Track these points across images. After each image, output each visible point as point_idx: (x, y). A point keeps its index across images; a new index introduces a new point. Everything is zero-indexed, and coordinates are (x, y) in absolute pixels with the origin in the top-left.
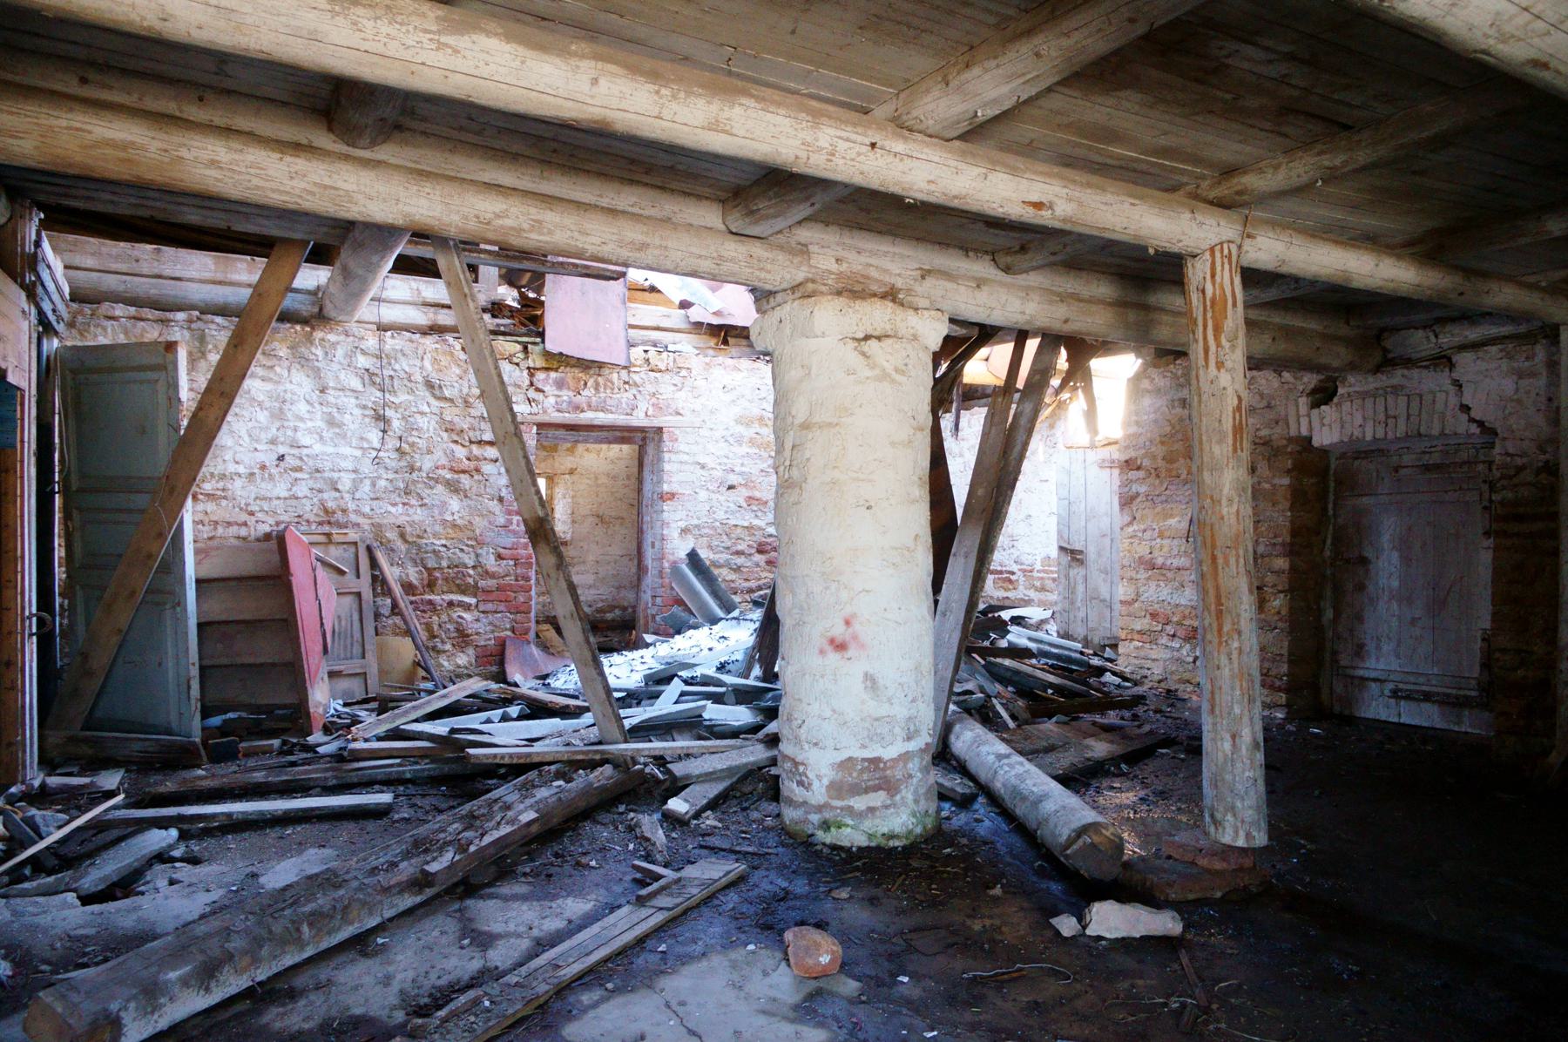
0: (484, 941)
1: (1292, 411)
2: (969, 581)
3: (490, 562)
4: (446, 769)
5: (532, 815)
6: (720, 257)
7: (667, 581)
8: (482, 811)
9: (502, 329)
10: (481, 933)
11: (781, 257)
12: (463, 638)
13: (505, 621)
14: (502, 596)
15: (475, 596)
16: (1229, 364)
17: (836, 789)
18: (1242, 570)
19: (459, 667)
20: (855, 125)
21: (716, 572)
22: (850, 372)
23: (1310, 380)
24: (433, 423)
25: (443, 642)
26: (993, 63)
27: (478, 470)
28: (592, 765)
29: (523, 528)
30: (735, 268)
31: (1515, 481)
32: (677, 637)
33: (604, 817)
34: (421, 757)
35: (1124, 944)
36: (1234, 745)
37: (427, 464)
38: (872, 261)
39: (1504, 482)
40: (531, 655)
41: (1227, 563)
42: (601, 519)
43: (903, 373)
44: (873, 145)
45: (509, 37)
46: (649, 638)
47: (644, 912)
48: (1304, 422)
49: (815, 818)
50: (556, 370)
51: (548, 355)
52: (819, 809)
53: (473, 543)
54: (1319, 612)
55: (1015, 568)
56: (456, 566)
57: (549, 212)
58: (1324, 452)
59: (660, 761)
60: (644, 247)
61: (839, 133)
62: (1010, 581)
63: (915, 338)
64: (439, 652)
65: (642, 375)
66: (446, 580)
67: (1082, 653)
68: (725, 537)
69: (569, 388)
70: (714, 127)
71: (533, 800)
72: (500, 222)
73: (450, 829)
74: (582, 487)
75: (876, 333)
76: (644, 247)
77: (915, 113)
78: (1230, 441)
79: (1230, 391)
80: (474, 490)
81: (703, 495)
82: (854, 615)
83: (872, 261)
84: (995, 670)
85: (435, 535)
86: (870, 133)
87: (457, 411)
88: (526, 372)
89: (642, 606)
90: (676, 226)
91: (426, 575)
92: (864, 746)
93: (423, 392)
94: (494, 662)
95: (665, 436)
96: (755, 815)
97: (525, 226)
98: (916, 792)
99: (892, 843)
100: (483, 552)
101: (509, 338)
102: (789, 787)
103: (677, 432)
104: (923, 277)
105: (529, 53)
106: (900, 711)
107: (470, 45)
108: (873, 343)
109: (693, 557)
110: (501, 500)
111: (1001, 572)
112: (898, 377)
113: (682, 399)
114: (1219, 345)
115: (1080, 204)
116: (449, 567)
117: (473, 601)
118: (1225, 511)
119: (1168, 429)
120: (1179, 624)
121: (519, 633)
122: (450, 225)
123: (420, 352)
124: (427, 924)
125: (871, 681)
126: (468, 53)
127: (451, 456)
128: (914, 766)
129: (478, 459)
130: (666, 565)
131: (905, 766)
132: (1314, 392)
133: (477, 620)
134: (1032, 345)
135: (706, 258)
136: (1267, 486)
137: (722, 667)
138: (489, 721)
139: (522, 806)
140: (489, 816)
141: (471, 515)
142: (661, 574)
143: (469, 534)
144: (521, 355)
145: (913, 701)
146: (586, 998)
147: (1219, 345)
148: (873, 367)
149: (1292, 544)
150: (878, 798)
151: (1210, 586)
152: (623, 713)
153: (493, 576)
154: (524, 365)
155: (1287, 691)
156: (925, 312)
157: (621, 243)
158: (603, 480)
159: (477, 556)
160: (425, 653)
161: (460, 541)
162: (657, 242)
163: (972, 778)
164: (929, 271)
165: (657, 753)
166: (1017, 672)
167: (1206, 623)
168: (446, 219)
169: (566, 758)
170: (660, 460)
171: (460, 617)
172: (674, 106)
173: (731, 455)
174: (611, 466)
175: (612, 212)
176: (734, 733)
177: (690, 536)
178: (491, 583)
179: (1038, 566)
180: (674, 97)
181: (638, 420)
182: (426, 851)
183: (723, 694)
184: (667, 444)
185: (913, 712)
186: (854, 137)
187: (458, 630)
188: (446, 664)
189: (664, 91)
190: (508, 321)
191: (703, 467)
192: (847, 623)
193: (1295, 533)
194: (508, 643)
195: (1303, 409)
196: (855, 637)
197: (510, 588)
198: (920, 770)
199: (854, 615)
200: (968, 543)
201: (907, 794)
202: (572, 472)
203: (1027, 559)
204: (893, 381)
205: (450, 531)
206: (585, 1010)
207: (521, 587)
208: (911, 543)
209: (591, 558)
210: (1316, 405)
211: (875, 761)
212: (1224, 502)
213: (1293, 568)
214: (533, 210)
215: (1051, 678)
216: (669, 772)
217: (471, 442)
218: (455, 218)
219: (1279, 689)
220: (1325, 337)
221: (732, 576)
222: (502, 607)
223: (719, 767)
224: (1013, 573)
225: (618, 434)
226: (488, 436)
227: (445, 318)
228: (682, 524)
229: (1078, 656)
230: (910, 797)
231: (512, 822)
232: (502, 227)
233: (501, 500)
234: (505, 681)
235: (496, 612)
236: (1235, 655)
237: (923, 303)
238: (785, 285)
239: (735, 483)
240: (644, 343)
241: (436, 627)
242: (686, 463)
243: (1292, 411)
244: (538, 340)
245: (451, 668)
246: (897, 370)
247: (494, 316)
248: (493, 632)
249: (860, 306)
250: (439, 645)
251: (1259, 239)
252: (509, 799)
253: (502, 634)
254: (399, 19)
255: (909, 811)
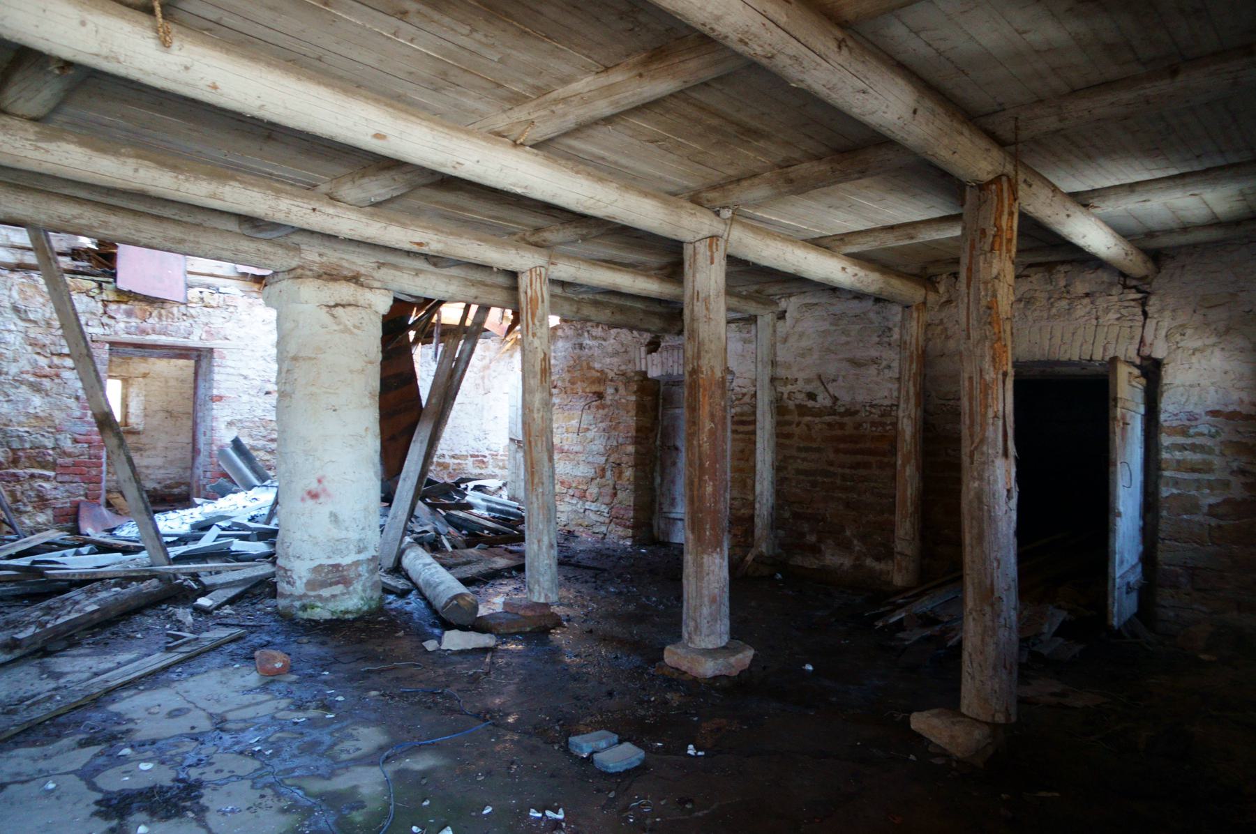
0: (58, 676)
1: (637, 356)
2: (422, 459)
3: (67, 444)
4: (28, 589)
5: (95, 607)
6: (237, 250)
7: (215, 460)
8: (57, 605)
9: (81, 269)
10: (55, 673)
11: (280, 251)
12: (42, 502)
13: (80, 489)
14: (77, 470)
15: (54, 470)
16: (539, 334)
17: (311, 585)
18: (545, 449)
19: (39, 524)
20: (303, 198)
21: (254, 454)
22: (323, 327)
23: (647, 337)
24: (19, 338)
25: (25, 505)
26: (374, 178)
27: (58, 376)
28: (141, 579)
29: (93, 420)
30: (248, 257)
31: (742, 402)
32: (220, 500)
33: (149, 612)
34: (8, 582)
35: (462, 653)
36: (539, 546)
37: (14, 369)
38: (343, 256)
39: (737, 402)
40: (101, 514)
41: (536, 445)
42: (170, 414)
43: (358, 328)
44: (314, 210)
45: (82, 144)
46: (198, 501)
47: (170, 655)
48: (643, 362)
49: (297, 604)
50: (126, 303)
51: (119, 292)
52: (300, 598)
53: (53, 430)
54: (653, 479)
55: (486, 453)
56: (38, 448)
57: (112, 216)
58: (656, 382)
59: (195, 576)
60: (182, 241)
61: (292, 202)
62: (483, 462)
63: (370, 306)
64: (21, 513)
65: (198, 310)
66: (28, 458)
67: (518, 509)
68: (262, 429)
69: (137, 317)
70: (213, 196)
71: (95, 599)
72: (77, 221)
73: (32, 615)
74: (153, 388)
75: (342, 303)
76: (182, 241)
77: (340, 193)
78: (539, 377)
79: (539, 350)
80: (54, 390)
81: (245, 398)
82: (324, 477)
83: (343, 256)
84: (452, 519)
85: (20, 424)
86: (312, 202)
87: (40, 330)
88: (100, 304)
89: (195, 479)
90: (206, 229)
91: (10, 454)
92: (329, 557)
93: (10, 315)
94: (70, 519)
95: (215, 355)
96: (260, 606)
97: (96, 225)
98: (364, 585)
99: (347, 616)
100: (61, 437)
101: (86, 277)
102: (283, 587)
103: (225, 352)
104: (379, 268)
105: (95, 154)
106: (354, 535)
107: (56, 148)
108: (340, 309)
109: (237, 444)
110: (77, 398)
111: (477, 456)
112: (356, 331)
113: (230, 328)
114: (534, 324)
115: (446, 244)
116: (31, 448)
117: (52, 474)
118: (536, 416)
119: (572, 362)
120: (576, 488)
121: (92, 498)
122: (39, 221)
123: (9, 284)
124: (16, 670)
125: (334, 518)
126: (55, 153)
127: (35, 364)
128: (363, 569)
129: (58, 367)
130: (215, 448)
131: (356, 569)
132: (650, 344)
133: (55, 488)
134: (474, 308)
135: (227, 250)
136: (623, 401)
137: (252, 519)
138: (64, 555)
139: (87, 602)
140: (63, 607)
141: (51, 409)
142: (210, 456)
143: (49, 423)
144: (97, 291)
145: (363, 529)
146: (125, 694)
147: (534, 324)
148: (339, 324)
149: (636, 437)
150: (338, 589)
151: (528, 457)
152: (169, 549)
153: (69, 455)
154: (98, 298)
155: (633, 527)
156: (378, 291)
157: (165, 238)
158: (172, 383)
159: (56, 440)
160: (9, 513)
161: (41, 428)
162: (192, 238)
163: (408, 578)
164: (383, 264)
165: (192, 571)
166: (465, 520)
168: (36, 217)
169: (123, 575)
170: (211, 372)
171: (40, 486)
172: (187, 185)
173: (268, 370)
174: (180, 372)
175: (159, 218)
176: (252, 558)
177: (234, 428)
178: (68, 460)
179: (501, 452)
180: (187, 180)
181: (194, 342)
182: (15, 627)
183: (248, 535)
184: (217, 360)
185: (363, 536)
186: (301, 204)
187: (38, 496)
188: (27, 521)
189: (180, 177)
190: (86, 264)
191: (245, 378)
192: (320, 481)
193: (638, 430)
194: (82, 505)
195: (643, 355)
196: (324, 490)
197: (85, 464)
198: (368, 572)
199: (324, 477)
200: (422, 434)
201: (358, 586)
202: (145, 376)
203: (494, 447)
204: (352, 333)
205: (32, 421)
206: (124, 699)
207: (94, 463)
208: (363, 433)
209: (160, 445)
210: (650, 352)
211: (336, 567)
212: (535, 411)
213: (637, 452)
214: (100, 215)
215: (489, 524)
216: (201, 583)
217: (52, 354)
218: (43, 217)
219: (629, 527)
220: (645, 312)
221: (268, 457)
222: (77, 479)
223: (237, 578)
224: (485, 457)
225: (178, 352)
226: (66, 350)
227: (31, 258)
228: (229, 419)
229: (515, 510)
230: (360, 588)
231: (80, 611)
232: (78, 224)
233: (77, 398)
234: (79, 534)
235: (72, 482)
236: (540, 496)
237: (376, 284)
238: (283, 269)
239: (271, 390)
240: (200, 286)
241: (19, 494)
242: (232, 374)
243: (637, 356)
244: (111, 280)
245: (32, 525)
246: (355, 327)
247: (74, 259)
248: (69, 497)
249: (332, 285)
250: (22, 508)
251: (560, 266)
252: (78, 598)
253: (77, 499)
254: (10, 132)
255: (358, 597)
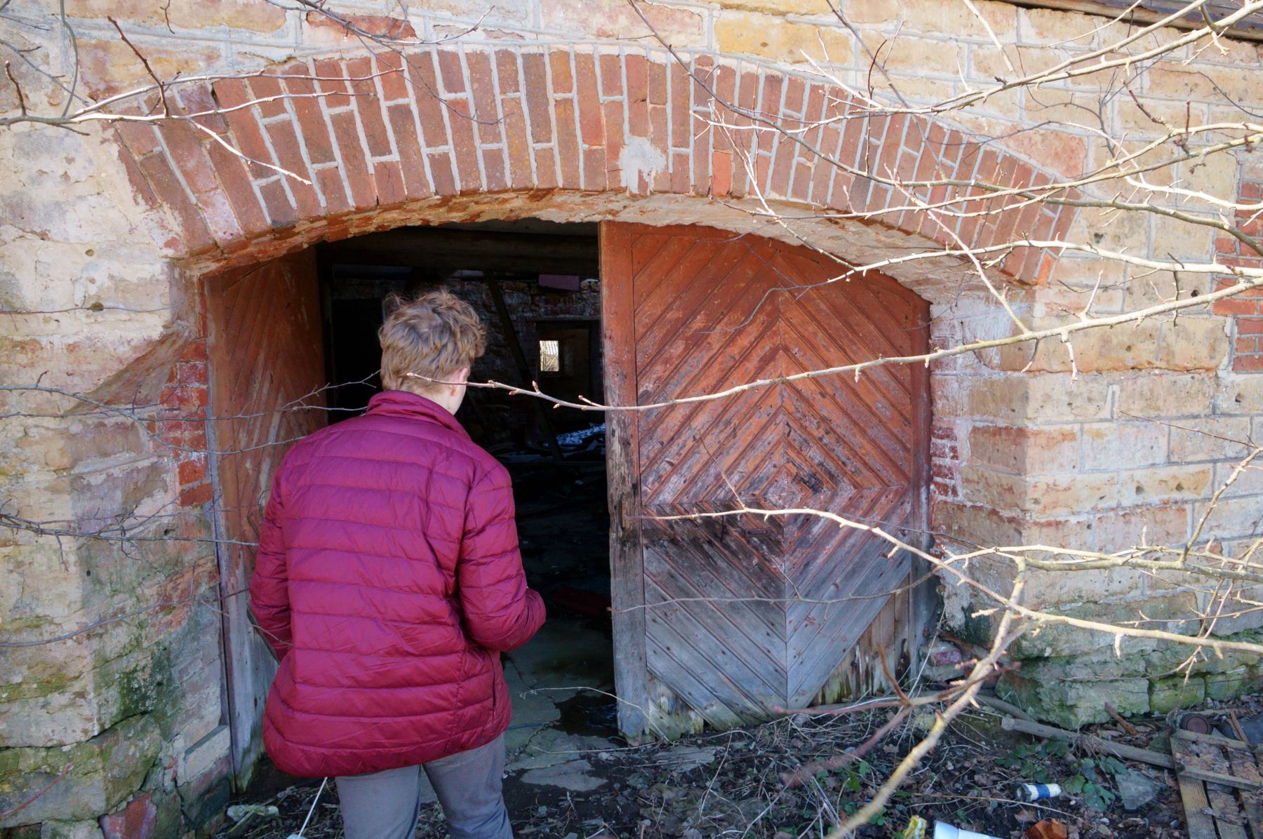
51: (540, 288)
167: (189, 558)
